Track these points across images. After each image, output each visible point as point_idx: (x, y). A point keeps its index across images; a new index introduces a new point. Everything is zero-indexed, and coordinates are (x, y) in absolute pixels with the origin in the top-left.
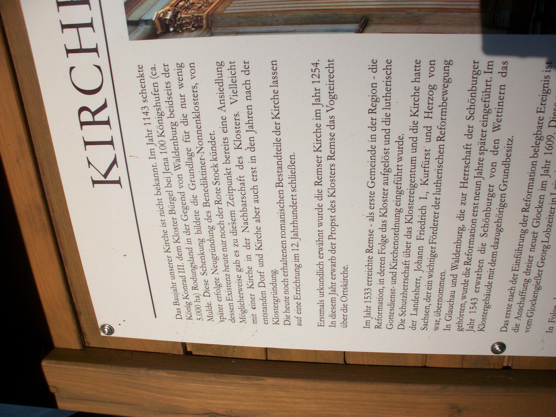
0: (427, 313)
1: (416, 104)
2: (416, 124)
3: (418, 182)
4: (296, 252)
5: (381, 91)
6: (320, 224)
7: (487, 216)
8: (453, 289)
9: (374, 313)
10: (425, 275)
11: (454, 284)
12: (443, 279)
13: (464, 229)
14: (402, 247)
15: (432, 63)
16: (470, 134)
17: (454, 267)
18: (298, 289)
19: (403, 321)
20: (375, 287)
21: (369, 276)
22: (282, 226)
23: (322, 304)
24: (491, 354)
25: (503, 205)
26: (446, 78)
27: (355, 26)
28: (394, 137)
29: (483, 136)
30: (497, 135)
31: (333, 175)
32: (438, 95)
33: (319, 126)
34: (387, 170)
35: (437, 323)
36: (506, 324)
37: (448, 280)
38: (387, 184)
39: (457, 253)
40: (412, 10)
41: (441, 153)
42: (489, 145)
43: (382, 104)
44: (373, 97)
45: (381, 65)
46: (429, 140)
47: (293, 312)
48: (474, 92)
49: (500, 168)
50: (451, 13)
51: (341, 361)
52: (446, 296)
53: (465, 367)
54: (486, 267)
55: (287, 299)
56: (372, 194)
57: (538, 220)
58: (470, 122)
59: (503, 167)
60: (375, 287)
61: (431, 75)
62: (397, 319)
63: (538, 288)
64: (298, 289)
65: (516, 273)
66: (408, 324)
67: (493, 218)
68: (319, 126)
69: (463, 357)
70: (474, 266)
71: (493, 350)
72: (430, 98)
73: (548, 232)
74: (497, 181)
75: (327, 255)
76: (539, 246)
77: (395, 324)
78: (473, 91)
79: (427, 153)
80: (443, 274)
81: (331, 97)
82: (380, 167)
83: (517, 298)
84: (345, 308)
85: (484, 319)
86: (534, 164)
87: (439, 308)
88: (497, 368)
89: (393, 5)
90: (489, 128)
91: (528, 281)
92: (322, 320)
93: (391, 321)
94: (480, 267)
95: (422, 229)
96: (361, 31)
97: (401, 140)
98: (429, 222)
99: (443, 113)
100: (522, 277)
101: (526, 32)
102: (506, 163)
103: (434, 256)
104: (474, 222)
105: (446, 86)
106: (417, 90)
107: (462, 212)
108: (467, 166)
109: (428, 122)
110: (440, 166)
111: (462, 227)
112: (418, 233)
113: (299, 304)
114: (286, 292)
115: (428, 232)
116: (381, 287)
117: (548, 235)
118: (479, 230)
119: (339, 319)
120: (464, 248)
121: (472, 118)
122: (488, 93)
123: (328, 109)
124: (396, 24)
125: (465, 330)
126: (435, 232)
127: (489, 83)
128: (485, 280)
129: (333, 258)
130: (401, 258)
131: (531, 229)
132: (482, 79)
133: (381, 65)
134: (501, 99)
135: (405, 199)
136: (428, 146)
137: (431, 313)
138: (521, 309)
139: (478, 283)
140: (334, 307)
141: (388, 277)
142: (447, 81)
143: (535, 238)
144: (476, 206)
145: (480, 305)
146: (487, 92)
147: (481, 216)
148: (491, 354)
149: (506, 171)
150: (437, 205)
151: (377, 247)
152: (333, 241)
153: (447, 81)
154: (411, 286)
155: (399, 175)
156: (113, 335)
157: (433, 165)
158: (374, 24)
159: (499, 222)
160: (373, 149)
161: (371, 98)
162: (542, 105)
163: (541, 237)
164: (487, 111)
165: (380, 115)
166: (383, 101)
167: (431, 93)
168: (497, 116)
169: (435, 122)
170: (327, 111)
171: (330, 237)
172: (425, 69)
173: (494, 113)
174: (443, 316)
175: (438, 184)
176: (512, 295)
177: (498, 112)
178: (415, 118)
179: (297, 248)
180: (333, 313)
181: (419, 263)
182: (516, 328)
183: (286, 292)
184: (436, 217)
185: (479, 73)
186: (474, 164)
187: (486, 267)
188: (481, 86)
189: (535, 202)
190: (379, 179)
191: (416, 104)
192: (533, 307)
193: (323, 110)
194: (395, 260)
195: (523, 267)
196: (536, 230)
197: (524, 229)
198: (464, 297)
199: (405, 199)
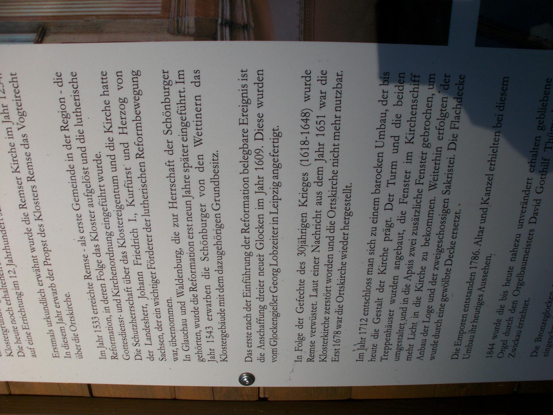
0: (162, 343)
1: (108, 119)
2: (111, 140)
3: (123, 203)
4: (15, 279)
5: (70, 107)
6: (33, 250)
7: (205, 238)
8: (184, 317)
9: (107, 343)
10: (151, 303)
11: (184, 312)
12: (170, 307)
13: (182, 253)
14: (121, 274)
15: (119, 75)
16: (170, 150)
17: (180, 294)
18: (25, 319)
19: (139, 352)
20: (102, 316)
21: (94, 304)
22: (192, 264)
23: (52, 333)
24: (240, 385)
25: (220, 227)
26: (135, 90)
27: (33, 36)
28: (91, 156)
29: (185, 152)
30: (200, 150)
31: (36, 197)
32: (130, 107)
33: (13, 146)
34: (90, 192)
35: (175, 353)
36: (250, 353)
37: (176, 308)
38: (92, 205)
39: (180, 278)
40: (90, 17)
41: (143, 171)
42: (193, 161)
43: (73, 120)
44: (64, 113)
45: (67, 78)
46: (127, 157)
47: (25, 344)
48: (383, 130)
49: (209, 187)
50: (132, 20)
51: (87, 394)
52: (178, 326)
53: (217, 399)
54: (215, 294)
55: (15, 329)
56: (79, 217)
57: (262, 242)
58: (169, 137)
59: (212, 185)
60: (102, 316)
61: (119, 87)
62: (132, 350)
63: (276, 315)
64: (25, 319)
65: (248, 299)
66: (145, 354)
67: (211, 241)
68: (13, 146)
69: (213, 389)
70: (201, 293)
71: (241, 380)
72: (123, 113)
73: (275, 254)
74: (209, 199)
75: (47, 282)
76: (268, 271)
77: (132, 355)
78: (166, 102)
79: (128, 171)
80: (169, 301)
81: (20, 114)
82: (82, 189)
83: (255, 327)
84: (76, 338)
85: (224, 349)
86: (246, 181)
87: (174, 338)
88: (252, 400)
89: (69, 12)
90: (190, 143)
91: (264, 308)
92: (56, 350)
93: (126, 352)
94: (208, 294)
95: (138, 253)
96: (40, 40)
97: (98, 158)
98: (144, 247)
99: (138, 128)
100: (256, 304)
101: (214, 38)
102: (215, 180)
103: (155, 282)
104: (191, 245)
105: (137, 98)
106: (107, 104)
107: (177, 235)
108: (173, 184)
109: (124, 138)
110: (144, 185)
111: (179, 251)
112: (135, 259)
113: (29, 335)
114: (13, 321)
115: (145, 257)
116: (108, 315)
117: (275, 258)
118: (199, 255)
119: (73, 350)
120: (187, 274)
121: (170, 132)
122: (183, 105)
123: (20, 126)
124: (75, 33)
125: (207, 361)
126: (330, 269)
127: (182, 94)
128: (216, 308)
129: (53, 285)
130: (122, 285)
131: (256, 252)
132: (174, 89)
133: (67, 78)
134: (199, 111)
135: (113, 221)
136: (128, 164)
137: (166, 343)
138: (262, 337)
139: (209, 311)
140: (64, 337)
141: (112, 305)
142: (138, 93)
143: (262, 261)
144: (190, 228)
145: (217, 334)
146: (182, 103)
147: (197, 238)
148: (240, 385)
149: (484, 216)
150: (148, 227)
151: (95, 274)
152: (50, 268)
153: (138, 93)
154: (139, 315)
155: (103, 196)
156: (254, 385)
157: (137, 184)
158: (53, 33)
159: (218, 244)
160: (72, 169)
161: (61, 114)
162: (243, 116)
163: (268, 260)
164: (185, 125)
165: (73, 132)
166: (73, 117)
167: (122, 107)
168: (197, 129)
169: (131, 138)
170: (19, 129)
171: (46, 263)
172: (112, 80)
173: (193, 126)
174: (179, 346)
175: (145, 204)
176: (249, 323)
177: (197, 125)
178: (109, 135)
179: (15, 275)
180: (65, 343)
181: (142, 289)
182: (262, 358)
183: (13, 321)
184: (150, 241)
185: (171, 84)
186: (180, 183)
187: (215, 294)
188: (175, 98)
189: (254, 222)
190: (84, 201)
191: (108, 119)
192: (275, 336)
193: (15, 128)
194: (116, 286)
195: (255, 293)
196: (261, 252)
197: (248, 251)
198: (197, 326)
199: (113, 221)
